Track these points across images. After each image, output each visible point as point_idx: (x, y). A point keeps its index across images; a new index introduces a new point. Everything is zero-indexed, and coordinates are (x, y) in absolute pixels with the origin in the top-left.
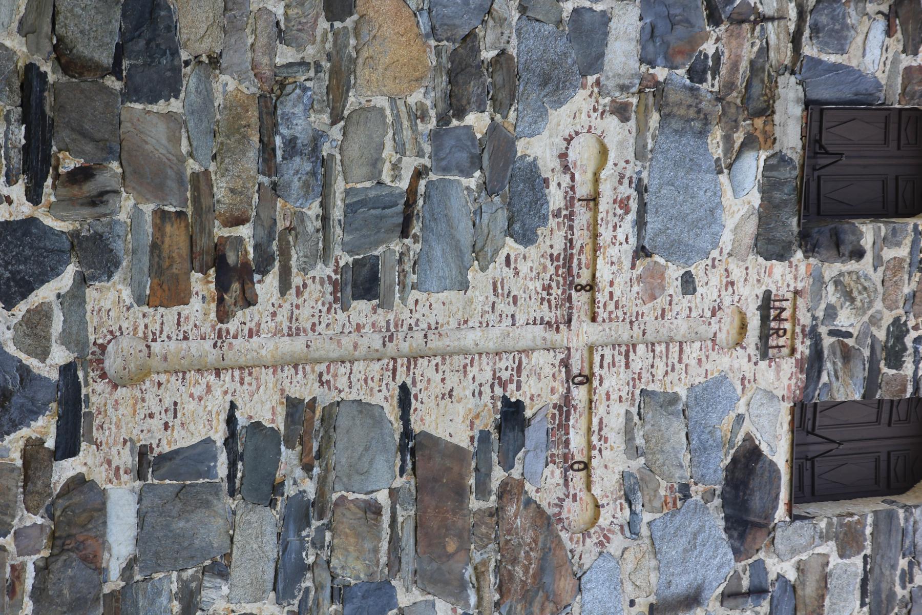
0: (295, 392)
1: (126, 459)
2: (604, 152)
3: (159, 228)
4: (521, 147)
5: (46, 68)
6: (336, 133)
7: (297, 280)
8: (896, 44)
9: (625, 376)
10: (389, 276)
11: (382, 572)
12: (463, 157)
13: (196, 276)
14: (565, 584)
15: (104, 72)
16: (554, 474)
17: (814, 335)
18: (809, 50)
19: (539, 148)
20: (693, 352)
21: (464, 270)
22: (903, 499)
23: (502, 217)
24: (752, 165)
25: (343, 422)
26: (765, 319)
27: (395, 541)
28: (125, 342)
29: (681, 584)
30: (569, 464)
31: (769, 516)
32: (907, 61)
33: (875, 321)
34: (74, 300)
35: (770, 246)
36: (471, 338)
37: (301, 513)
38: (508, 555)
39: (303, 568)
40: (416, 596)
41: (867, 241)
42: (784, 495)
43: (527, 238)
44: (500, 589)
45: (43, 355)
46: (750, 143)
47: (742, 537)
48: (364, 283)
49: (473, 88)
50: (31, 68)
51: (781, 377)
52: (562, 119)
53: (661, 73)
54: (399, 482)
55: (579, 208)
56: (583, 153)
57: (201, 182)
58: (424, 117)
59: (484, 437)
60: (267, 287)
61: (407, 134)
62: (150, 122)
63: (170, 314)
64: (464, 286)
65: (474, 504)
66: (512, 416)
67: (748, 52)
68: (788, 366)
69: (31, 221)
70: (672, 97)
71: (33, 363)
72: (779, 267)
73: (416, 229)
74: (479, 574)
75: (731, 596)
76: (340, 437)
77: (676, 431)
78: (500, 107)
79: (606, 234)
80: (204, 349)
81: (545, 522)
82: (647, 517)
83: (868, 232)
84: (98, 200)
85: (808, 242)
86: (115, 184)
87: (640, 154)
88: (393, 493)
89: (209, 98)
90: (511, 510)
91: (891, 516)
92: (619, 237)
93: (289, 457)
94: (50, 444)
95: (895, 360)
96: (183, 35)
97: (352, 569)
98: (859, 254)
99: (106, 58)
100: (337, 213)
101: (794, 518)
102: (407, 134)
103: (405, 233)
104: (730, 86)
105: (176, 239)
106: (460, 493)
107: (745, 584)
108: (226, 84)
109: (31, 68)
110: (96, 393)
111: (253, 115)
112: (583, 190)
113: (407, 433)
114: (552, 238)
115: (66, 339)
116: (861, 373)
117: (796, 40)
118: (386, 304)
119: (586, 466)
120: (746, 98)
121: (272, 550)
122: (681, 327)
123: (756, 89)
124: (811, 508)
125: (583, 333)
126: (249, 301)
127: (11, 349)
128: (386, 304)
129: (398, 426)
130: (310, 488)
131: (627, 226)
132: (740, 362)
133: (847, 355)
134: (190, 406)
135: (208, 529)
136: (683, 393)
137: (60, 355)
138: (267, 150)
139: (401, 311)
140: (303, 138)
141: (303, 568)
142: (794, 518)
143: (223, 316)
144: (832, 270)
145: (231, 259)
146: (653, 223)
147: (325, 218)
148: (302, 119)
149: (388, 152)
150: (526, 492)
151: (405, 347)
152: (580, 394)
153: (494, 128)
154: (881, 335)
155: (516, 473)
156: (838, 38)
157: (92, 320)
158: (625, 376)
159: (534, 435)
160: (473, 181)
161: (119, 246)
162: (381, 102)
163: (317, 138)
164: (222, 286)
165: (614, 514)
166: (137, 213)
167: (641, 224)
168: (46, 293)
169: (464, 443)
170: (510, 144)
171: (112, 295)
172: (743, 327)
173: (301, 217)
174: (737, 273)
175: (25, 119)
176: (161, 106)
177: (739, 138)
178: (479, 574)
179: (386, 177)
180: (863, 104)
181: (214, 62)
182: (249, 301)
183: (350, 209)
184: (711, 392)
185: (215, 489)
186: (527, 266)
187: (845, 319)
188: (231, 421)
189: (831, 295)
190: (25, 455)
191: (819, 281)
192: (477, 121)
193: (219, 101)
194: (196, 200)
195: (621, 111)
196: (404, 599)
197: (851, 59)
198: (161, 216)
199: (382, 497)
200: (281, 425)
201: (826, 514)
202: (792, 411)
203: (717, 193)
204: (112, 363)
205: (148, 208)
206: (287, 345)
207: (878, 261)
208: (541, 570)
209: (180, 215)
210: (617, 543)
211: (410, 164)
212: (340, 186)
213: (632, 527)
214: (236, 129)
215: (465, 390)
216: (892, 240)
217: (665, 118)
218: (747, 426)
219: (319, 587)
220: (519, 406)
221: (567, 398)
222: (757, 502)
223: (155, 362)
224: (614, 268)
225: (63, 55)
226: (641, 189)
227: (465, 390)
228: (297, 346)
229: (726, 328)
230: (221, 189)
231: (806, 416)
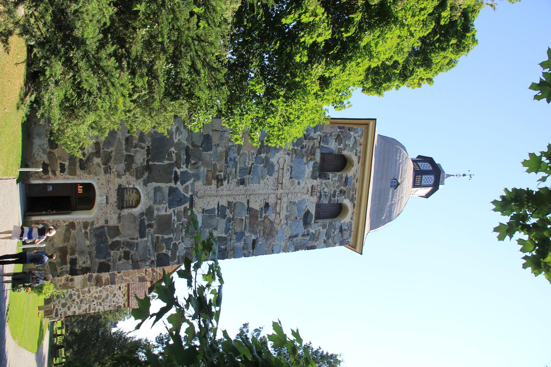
0: (229, 200)
1: (201, 210)
2: (285, 161)
3: (207, 173)
4: (270, 160)
5: (190, 146)
6: (238, 157)
7: (230, 182)
8: (337, 144)
9: (287, 199)
10: (246, 181)
11: (243, 230)
12: (260, 161)
13: (213, 181)
14: (275, 233)
15: (199, 147)
16: (273, 215)
17: (320, 192)
18: (322, 144)
19: (274, 160)
20: (299, 195)
21: (259, 180)
22: (334, 219)
23: (267, 171)
24: (311, 164)
25: (237, 205)
26: (312, 189)
27: (245, 225)
28: (201, 191)
29: (295, 233)
30: (276, 213)
31: (311, 222)
32: (339, 147)
33: (331, 190)
34: (193, 184)
35: (314, 177)
36: (260, 192)
37: (229, 220)
38: (265, 228)
39: (229, 229)
40: (249, 234)
41: (330, 177)
42: (313, 219)
43: (271, 175)
44: (263, 233)
45: (187, 193)
46: (311, 160)
47: (306, 226)
48: (242, 182)
49: (263, 150)
50: (187, 146)
51: (314, 199)
52: (278, 155)
53: (296, 148)
54: (247, 216)
55: (280, 170)
56: (282, 161)
57: (215, 165)
58: (254, 155)
59: (262, 208)
60: (225, 183)
61: (251, 157)
62: (207, 155)
63: (209, 187)
64: (259, 183)
65: (259, 219)
66: (267, 205)
67: (311, 144)
68: (316, 197)
69: (186, 171)
70: (298, 152)
71: (186, 194)
72: (315, 181)
73: (251, 173)
74: (260, 231)
75: (303, 235)
76: (237, 208)
77: (295, 208)
78: (267, 153)
79: (285, 175)
80: (214, 193)
81: (272, 223)
82: (289, 222)
83: (331, 175)
84: (197, 168)
85: (320, 176)
86: (200, 165)
87: (291, 161)
88: (245, 217)
89: (217, 151)
90: (266, 221)
91: (332, 223)
92: (287, 175)
93: (228, 211)
94: (188, 208)
95: (334, 196)
96: (213, 141)
97: (238, 230)
98: (329, 179)
99: (200, 145)
100: (238, 170)
101: (315, 222)
102: (251, 157)
103: (249, 174)
104: (308, 150)
105: (210, 174)
106: (257, 218)
107: (306, 233)
108: (220, 149)
109: (187, 146)
110: (196, 199)
111: (224, 154)
112: (281, 167)
113: (248, 207)
114: (275, 175)
115: (191, 191)
116: (328, 199)
117: (320, 143)
118: (246, 186)
119: (279, 213)
120: (311, 152)
121: (224, 226)
122: (297, 191)
123: (312, 151)
124: (319, 221)
125: (280, 191)
126: (222, 185)
127: (182, 192)
128: (246, 186)
129: (247, 206)
130: (231, 216)
131: (289, 173)
132: (307, 197)
133: (326, 196)
134: (211, 202)
135: (214, 222)
136: (297, 202)
137: (190, 193)
138: (226, 160)
139: (248, 187)
140: (233, 158)
141: (229, 229)
142: (315, 222)
143: (218, 187)
144: (324, 181)
145: (219, 178)
146: (293, 173)
147: (236, 171)
148: (232, 155)
149: (247, 160)
150: (377, 67)
151: (249, 193)
152: (279, 201)
153: (266, 156)
154: (332, 192)
155: (267, 215)
156: (327, 142)
157: (196, 188)
158: (287, 199)
159: (270, 208)
160: (262, 166)
161: (200, 175)
162: (246, 152)
163: (235, 158)
164: (218, 182)
165: (284, 221)
166: (204, 170)
167: (291, 173)
168: (188, 183)
169: (258, 209)
170: (269, 159)
171: (199, 184)
172: (308, 191)
173: (232, 171)
174: (307, 182)
175: (186, 155)
176: (209, 152)
177: (309, 159)
178: (260, 231)
179: (247, 164)
180: (331, 153)
181: (218, 145)
182: (222, 185)
183: (240, 170)
184: (302, 202)
185: (215, 216)
186: (270, 180)
187: (326, 190)
188: (218, 205)
189: (324, 186)
190: (184, 210)
191: (322, 183)
192: (263, 155)
193: (218, 152)
194: (214, 168)
195: (288, 154)
196: (247, 235)
197: (329, 146)
198: (208, 170)
199: (244, 218)
200: (227, 206)
201: (321, 222)
202: (316, 205)
203: (305, 168)
204: (199, 195)
205: (206, 169)
206: (229, 192)
207: (332, 180)
208: (271, 230)
209: (211, 170)
210: (284, 226)
211: (251, 163)
212: (238, 166)
213: (287, 224)
214: (221, 156)
215: (259, 200)
216: (335, 177)
217: (296, 155)
218: (308, 207)
219: (232, 232)
220: (268, 203)
221: (277, 202)
222: (309, 220)
223: (206, 195)
224: (286, 180)
225: (193, 145)
226: (291, 167)
227: (259, 200)
228: (230, 192)
229: (305, 191)
230: (218, 166)
231: (318, 206)
